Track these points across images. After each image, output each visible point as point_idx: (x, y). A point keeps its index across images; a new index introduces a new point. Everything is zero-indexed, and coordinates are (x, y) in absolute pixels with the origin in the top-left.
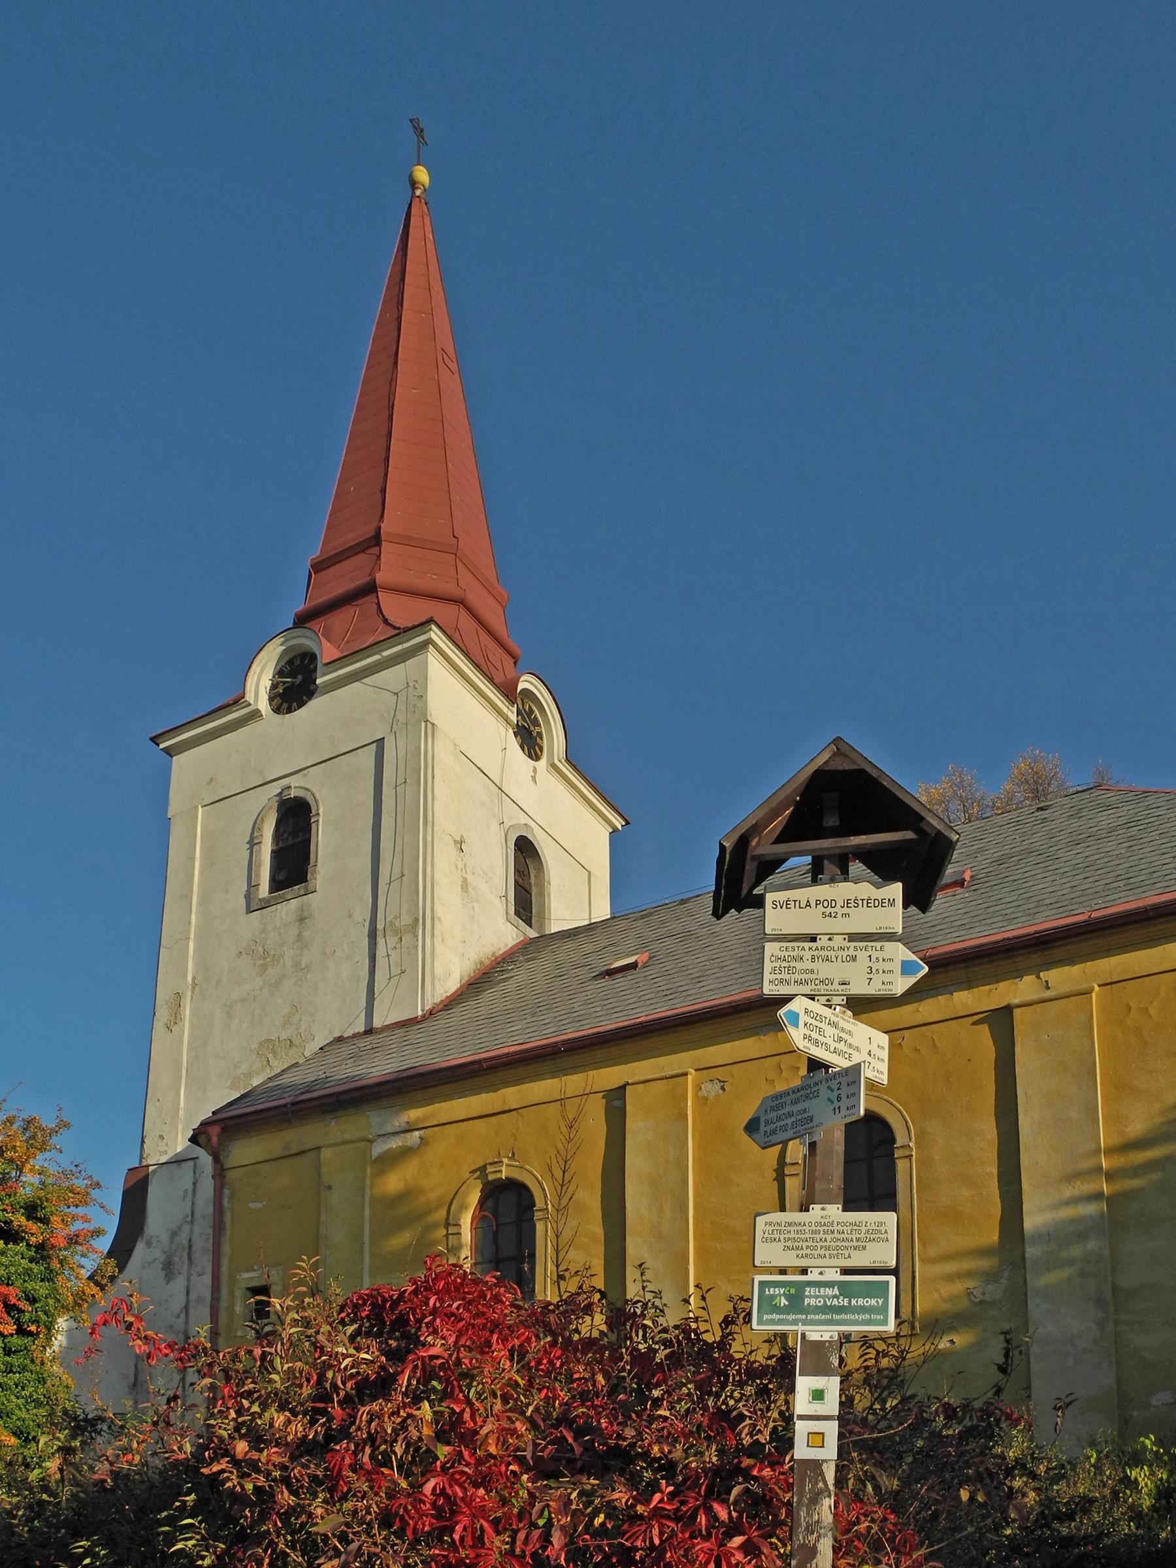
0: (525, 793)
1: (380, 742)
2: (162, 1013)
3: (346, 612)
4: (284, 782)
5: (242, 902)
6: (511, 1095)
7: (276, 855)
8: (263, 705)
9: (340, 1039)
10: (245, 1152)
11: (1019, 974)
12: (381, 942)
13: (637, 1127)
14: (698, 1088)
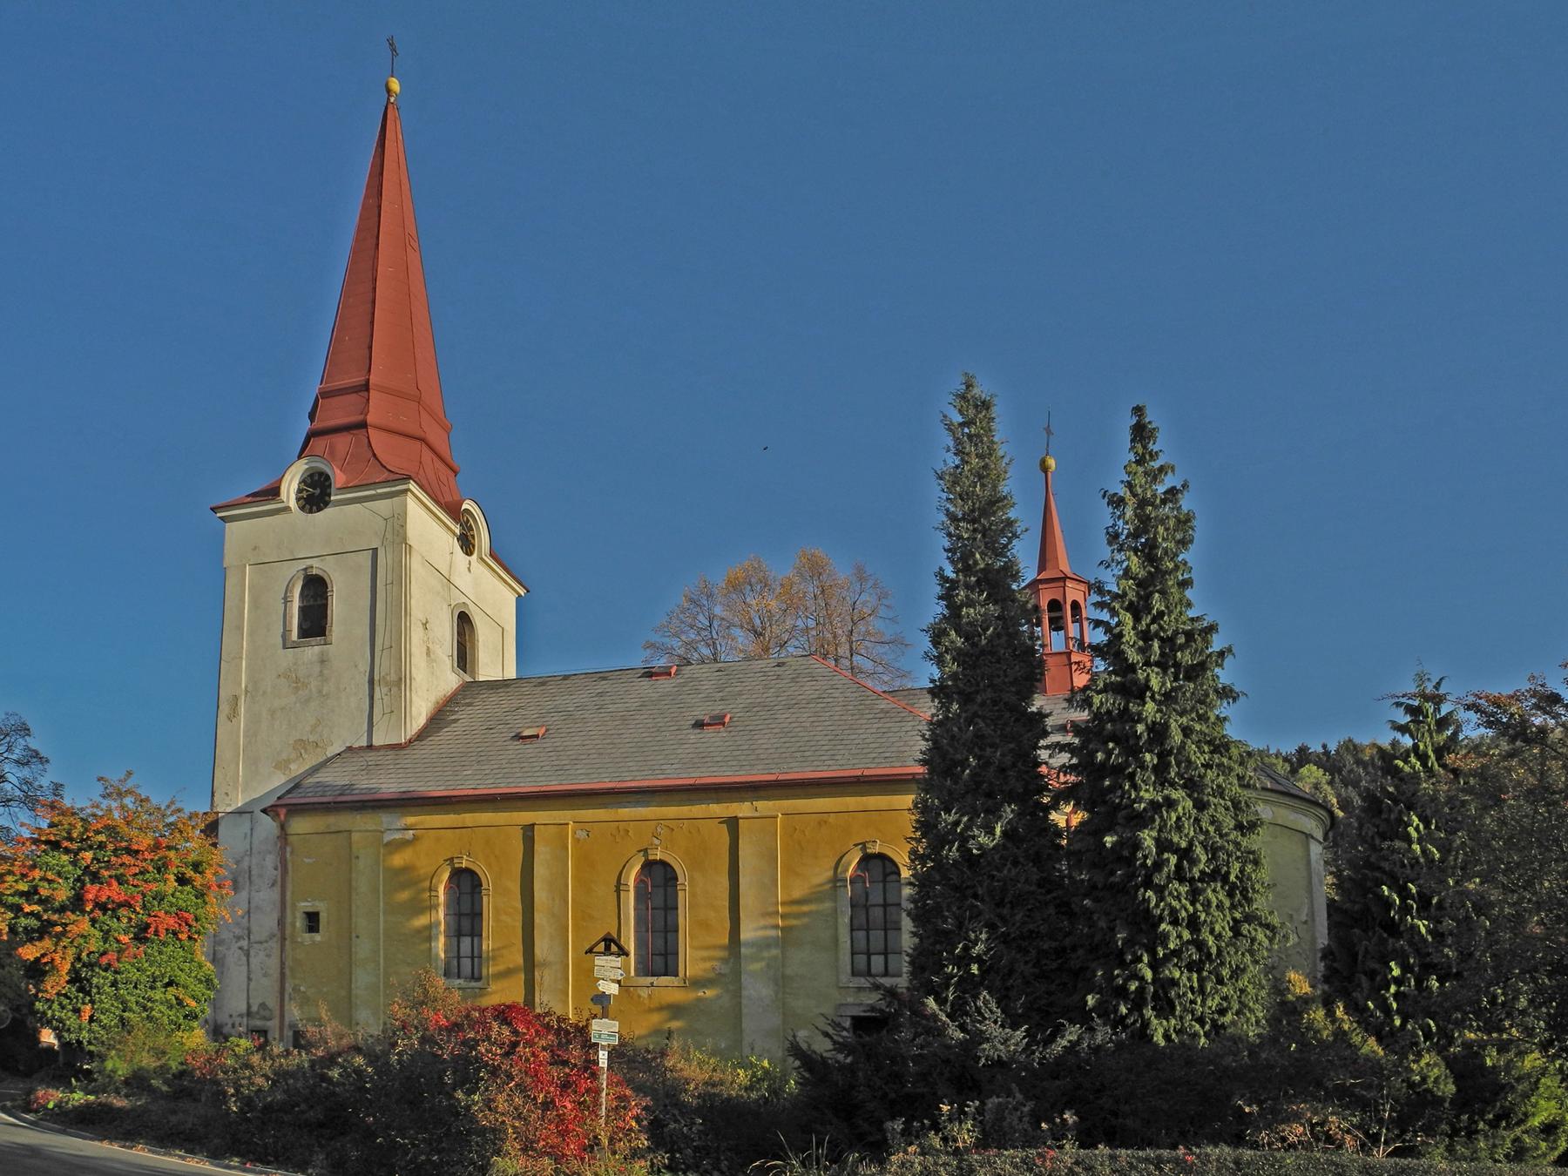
0: (462, 580)
1: (375, 550)
2: (225, 708)
3: (351, 443)
4: (309, 562)
5: (280, 640)
6: (469, 818)
7: (302, 610)
8: (293, 503)
9: (350, 749)
10: (300, 826)
11: (743, 800)
12: (377, 689)
13: (542, 852)
14: (574, 833)
